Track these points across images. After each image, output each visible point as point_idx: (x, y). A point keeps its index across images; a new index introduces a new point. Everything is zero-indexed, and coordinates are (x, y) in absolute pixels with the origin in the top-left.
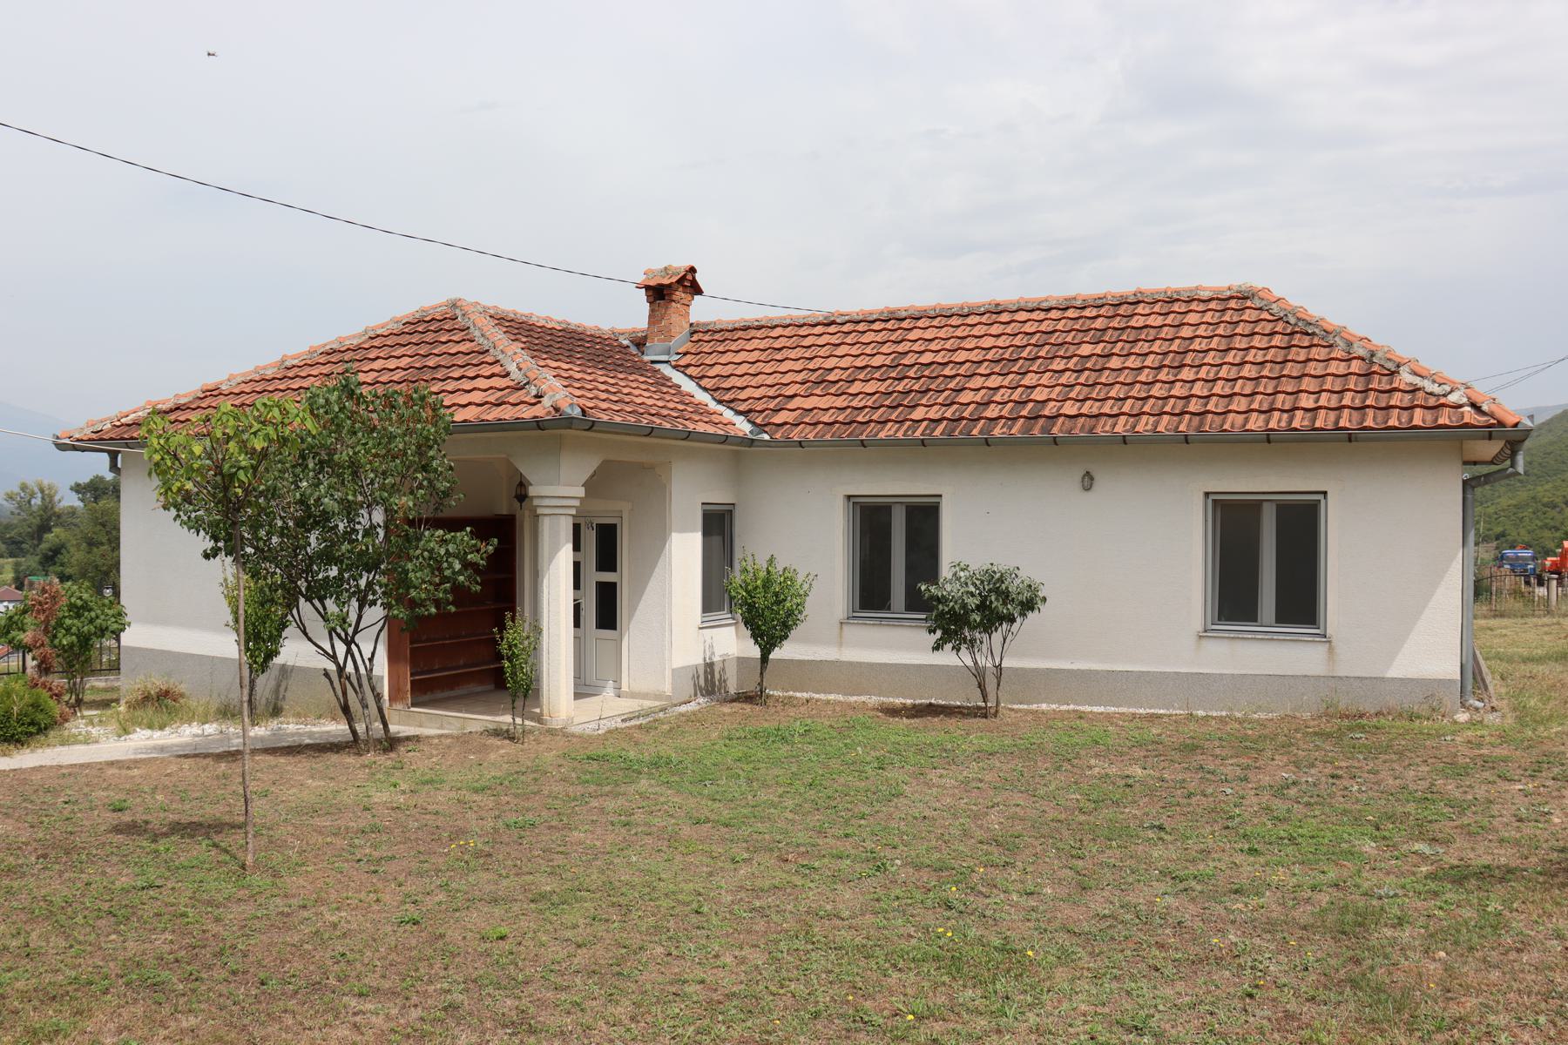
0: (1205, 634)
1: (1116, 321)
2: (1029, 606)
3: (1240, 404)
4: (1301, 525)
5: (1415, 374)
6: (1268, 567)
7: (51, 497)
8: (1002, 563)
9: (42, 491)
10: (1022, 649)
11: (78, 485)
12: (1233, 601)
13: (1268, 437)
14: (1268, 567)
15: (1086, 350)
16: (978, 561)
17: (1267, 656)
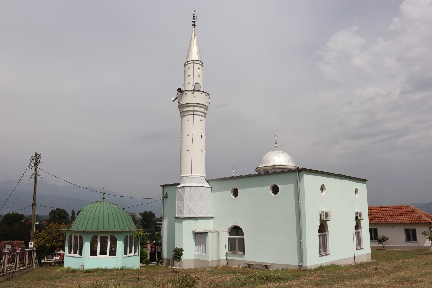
0: (406, 242)
1: (394, 210)
2: (387, 239)
3: (406, 220)
4: (414, 231)
5: (323, 228)
6: (411, 236)
7: (135, 216)
8: (384, 235)
9: (133, 215)
10: (387, 244)
11: (141, 213)
12: (408, 239)
13: (409, 224)
14: (411, 236)
15: (391, 213)
16: (382, 235)
17: (412, 244)
